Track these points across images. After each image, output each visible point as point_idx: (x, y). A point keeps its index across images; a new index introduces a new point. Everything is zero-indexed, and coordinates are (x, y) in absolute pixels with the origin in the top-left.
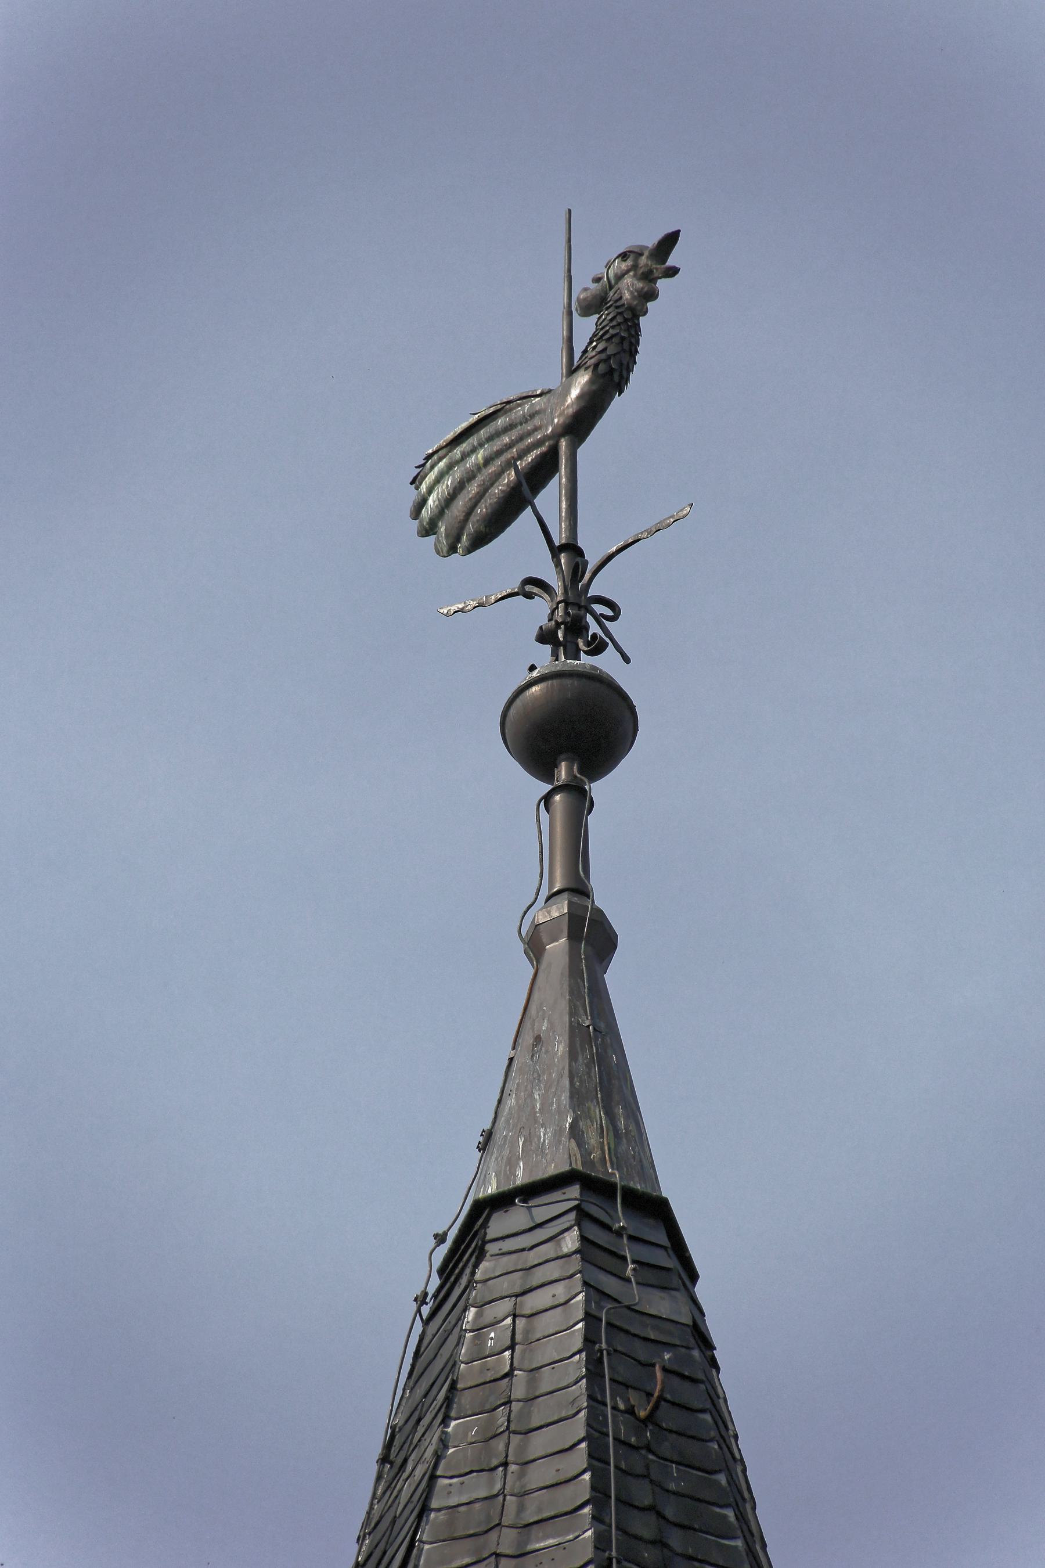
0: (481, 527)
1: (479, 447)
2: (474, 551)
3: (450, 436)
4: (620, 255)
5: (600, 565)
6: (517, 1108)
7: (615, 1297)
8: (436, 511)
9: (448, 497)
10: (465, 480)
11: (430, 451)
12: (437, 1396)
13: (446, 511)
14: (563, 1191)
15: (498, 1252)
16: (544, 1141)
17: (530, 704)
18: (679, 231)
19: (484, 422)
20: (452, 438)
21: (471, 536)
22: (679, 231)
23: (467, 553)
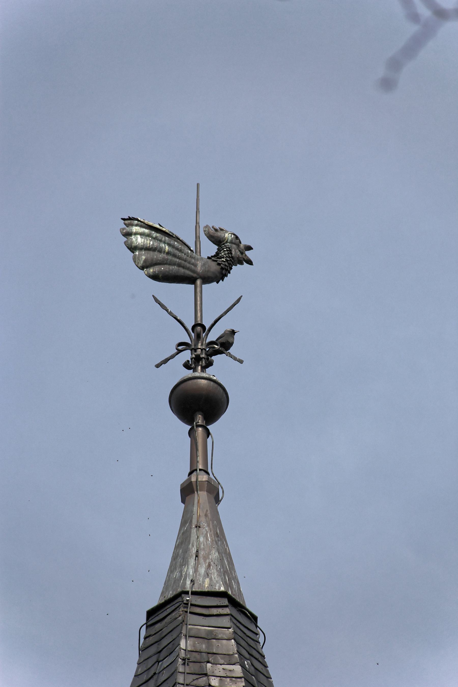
0: (161, 275)
1: (163, 242)
2: (151, 278)
3: (151, 224)
4: (237, 238)
5: (186, 328)
6: (203, 549)
7: (159, 630)
8: (140, 246)
9: (148, 247)
10: (158, 249)
11: (139, 219)
12: (263, 685)
13: (143, 250)
14: (241, 614)
15: (235, 623)
16: (179, 559)
17: (211, 388)
18: (252, 249)
19: (166, 235)
20: (151, 225)
21: (155, 273)
22: (252, 249)
23: (149, 276)
